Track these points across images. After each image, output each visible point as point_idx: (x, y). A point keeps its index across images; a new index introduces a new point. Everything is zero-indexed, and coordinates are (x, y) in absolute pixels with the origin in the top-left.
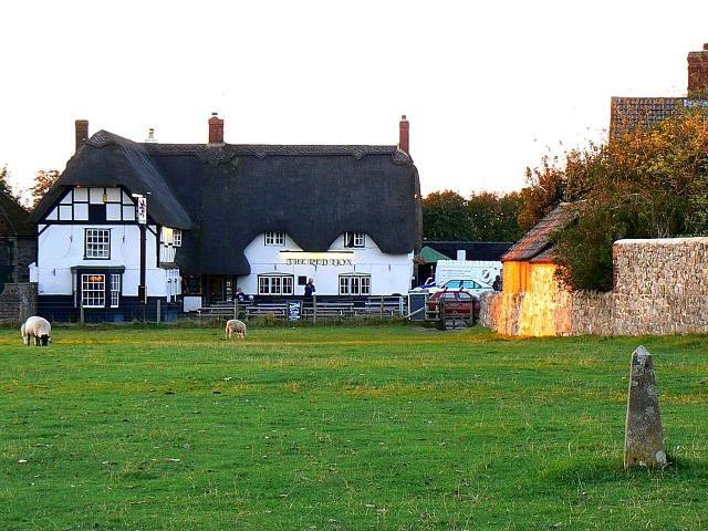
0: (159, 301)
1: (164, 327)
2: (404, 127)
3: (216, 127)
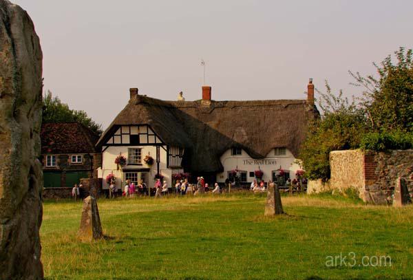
0: (139, 174)
1: (130, 199)
2: (311, 88)
3: (207, 91)
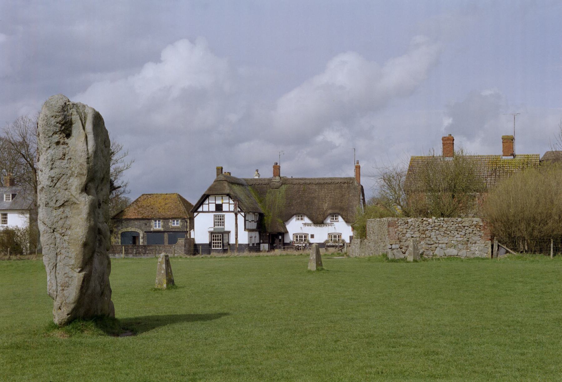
3: (277, 168)
